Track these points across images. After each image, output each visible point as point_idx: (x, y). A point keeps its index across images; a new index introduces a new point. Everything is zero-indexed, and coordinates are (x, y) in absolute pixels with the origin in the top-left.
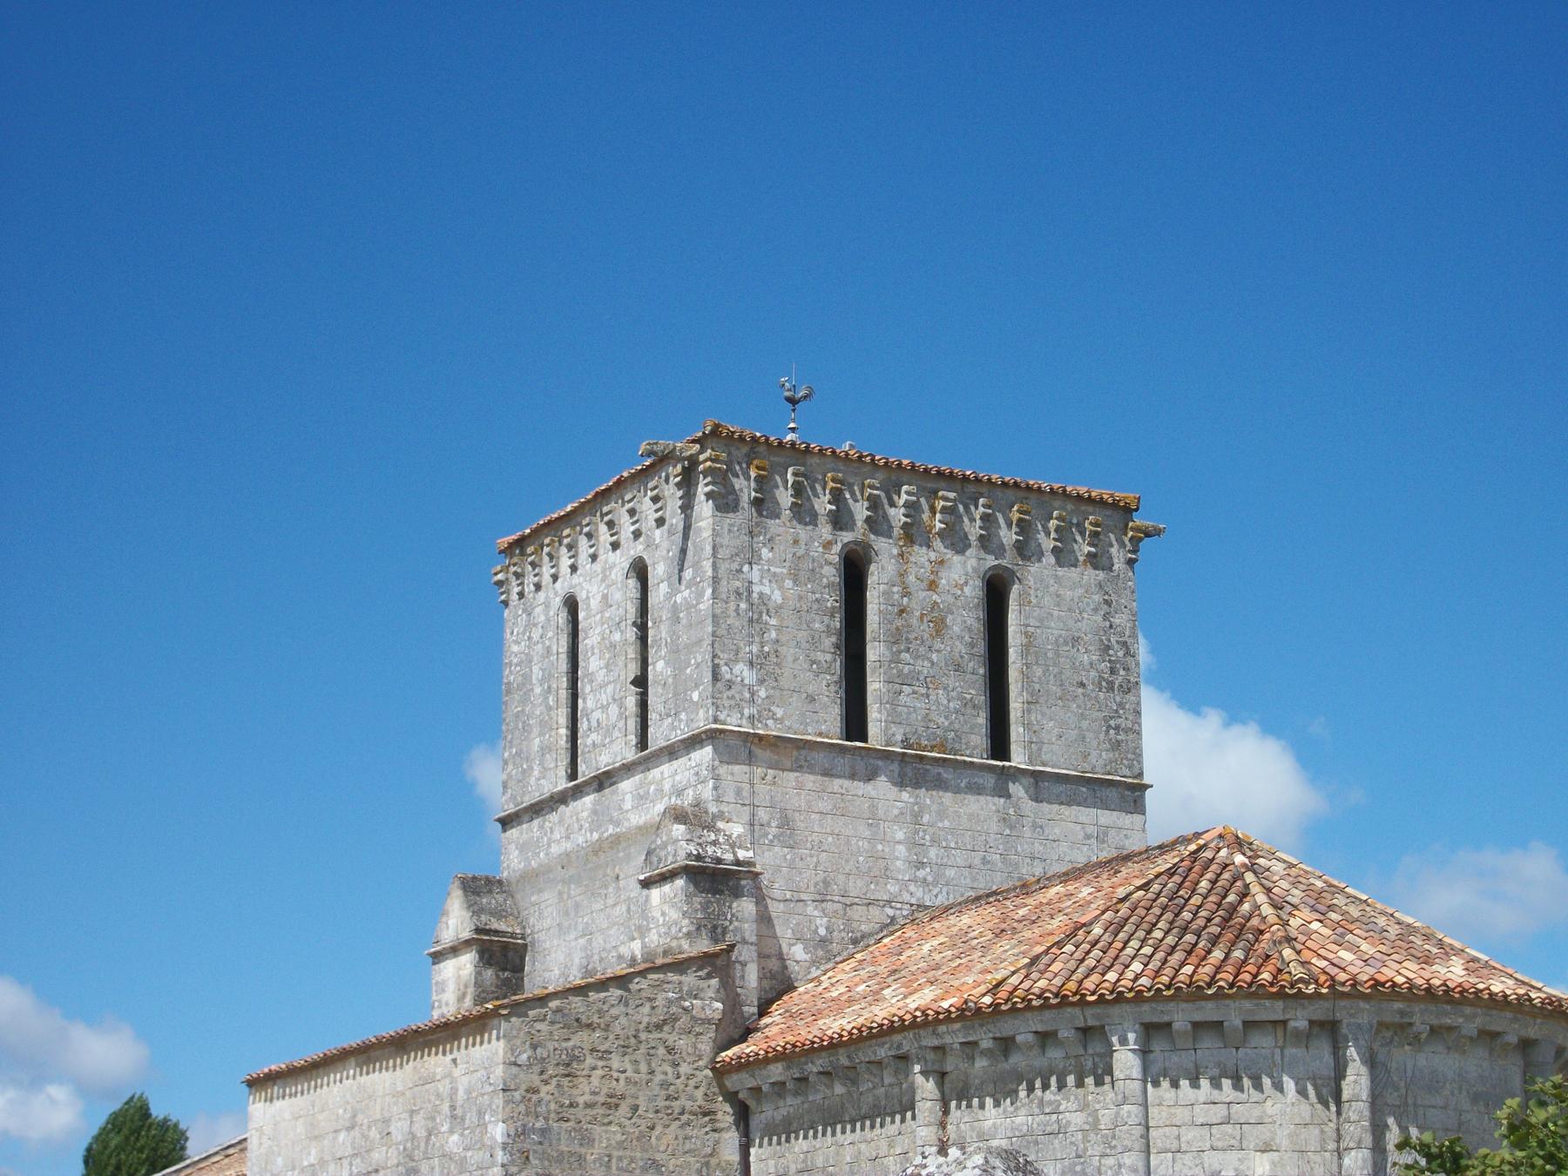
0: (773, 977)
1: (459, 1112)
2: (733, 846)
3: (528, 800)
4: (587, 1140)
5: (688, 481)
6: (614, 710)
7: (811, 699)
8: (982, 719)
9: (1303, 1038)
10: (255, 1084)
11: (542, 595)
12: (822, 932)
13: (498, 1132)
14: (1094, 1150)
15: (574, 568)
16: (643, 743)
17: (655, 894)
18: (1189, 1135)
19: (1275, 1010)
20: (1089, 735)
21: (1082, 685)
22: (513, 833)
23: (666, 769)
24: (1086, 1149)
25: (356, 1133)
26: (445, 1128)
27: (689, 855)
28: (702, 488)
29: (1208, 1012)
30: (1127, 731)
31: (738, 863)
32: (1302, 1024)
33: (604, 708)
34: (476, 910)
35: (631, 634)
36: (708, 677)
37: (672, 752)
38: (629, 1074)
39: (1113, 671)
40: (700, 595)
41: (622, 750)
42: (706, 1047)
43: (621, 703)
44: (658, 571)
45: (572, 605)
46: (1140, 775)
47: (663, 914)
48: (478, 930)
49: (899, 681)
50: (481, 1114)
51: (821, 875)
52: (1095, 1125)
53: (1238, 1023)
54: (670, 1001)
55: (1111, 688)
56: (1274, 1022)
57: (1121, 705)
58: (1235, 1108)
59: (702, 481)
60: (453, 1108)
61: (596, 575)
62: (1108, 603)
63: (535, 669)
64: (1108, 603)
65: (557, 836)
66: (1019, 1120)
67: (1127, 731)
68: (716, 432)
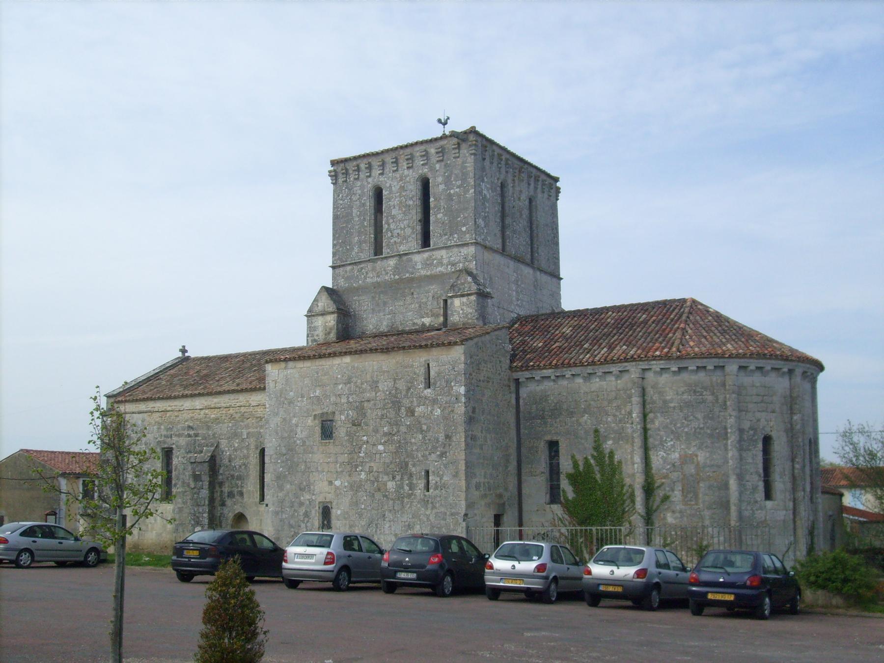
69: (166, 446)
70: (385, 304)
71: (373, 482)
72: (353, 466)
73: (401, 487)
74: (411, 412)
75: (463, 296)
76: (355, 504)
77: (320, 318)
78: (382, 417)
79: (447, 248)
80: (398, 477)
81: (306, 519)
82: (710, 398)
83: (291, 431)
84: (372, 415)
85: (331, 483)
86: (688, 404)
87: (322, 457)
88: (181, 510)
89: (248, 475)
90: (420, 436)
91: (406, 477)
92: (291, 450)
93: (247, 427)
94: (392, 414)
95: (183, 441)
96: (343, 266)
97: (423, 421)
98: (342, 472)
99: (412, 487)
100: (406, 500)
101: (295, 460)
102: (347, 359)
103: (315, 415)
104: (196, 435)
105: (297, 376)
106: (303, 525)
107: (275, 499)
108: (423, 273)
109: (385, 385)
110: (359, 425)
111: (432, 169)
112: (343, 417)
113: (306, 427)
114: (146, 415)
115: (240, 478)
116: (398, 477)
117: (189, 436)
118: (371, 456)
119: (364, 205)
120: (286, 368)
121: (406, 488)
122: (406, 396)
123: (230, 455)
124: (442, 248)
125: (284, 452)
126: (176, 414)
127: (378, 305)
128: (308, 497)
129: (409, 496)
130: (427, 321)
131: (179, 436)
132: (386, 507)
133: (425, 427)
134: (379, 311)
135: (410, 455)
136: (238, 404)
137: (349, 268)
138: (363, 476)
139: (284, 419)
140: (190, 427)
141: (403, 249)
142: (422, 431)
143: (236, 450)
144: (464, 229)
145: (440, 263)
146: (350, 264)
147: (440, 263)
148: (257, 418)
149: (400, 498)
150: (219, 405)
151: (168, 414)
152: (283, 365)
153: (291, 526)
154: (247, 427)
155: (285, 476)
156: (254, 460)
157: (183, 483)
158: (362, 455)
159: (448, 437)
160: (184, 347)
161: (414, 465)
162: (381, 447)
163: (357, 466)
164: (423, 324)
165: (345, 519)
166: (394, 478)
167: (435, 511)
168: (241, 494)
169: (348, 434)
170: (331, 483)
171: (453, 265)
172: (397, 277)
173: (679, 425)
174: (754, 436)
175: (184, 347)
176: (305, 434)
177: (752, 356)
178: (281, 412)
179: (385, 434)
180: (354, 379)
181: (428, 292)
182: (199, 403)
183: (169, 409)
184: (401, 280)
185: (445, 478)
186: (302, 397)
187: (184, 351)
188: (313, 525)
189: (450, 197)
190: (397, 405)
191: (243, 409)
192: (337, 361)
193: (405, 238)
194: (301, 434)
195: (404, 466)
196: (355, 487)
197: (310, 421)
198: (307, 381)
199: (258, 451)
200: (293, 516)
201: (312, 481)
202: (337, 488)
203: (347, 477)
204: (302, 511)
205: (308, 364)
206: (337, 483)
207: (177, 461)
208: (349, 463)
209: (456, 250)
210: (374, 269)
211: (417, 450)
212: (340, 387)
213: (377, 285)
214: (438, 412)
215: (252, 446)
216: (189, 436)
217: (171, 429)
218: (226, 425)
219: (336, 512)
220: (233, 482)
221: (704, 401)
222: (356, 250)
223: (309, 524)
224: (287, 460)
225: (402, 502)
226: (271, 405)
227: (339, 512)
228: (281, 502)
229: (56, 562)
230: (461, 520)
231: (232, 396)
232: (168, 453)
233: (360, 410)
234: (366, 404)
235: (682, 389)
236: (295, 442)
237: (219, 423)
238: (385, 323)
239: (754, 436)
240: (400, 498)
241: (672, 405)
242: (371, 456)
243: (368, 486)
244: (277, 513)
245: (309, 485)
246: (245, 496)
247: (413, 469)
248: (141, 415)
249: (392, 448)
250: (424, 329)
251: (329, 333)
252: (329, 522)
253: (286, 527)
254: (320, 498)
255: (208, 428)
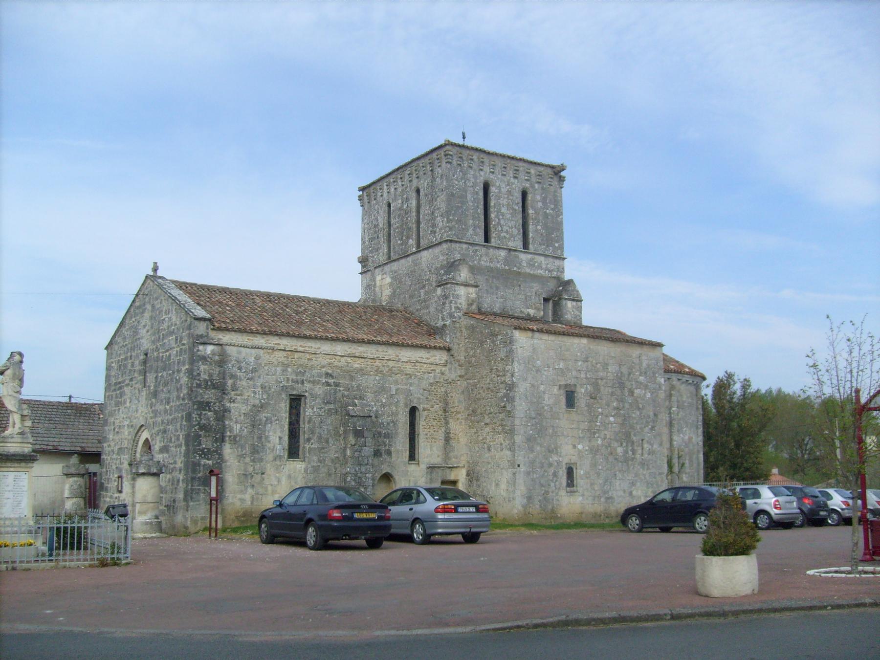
69: (295, 393)
70: (497, 288)
71: (607, 447)
72: (592, 433)
73: (626, 452)
74: (631, 393)
75: (573, 300)
76: (594, 465)
77: (462, 287)
78: (612, 394)
79: (546, 256)
80: (624, 444)
81: (555, 479)
83: (540, 397)
84: (605, 391)
85: (574, 446)
87: (568, 424)
88: (316, 469)
89: (397, 434)
90: (638, 413)
91: (630, 444)
92: (540, 415)
93: (396, 382)
94: (618, 392)
95: (319, 390)
96: (460, 242)
97: (639, 400)
98: (583, 437)
99: (634, 452)
100: (630, 463)
101: (544, 424)
102: (584, 341)
103: (560, 385)
104: (337, 385)
105: (543, 347)
106: (552, 484)
107: (526, 459)
108: (528, 270)
109: (612, 368)
110: (595, 399)
111: (532, 186)
112: (583, 390)
113: (553, 397)
114: (261, 352)
115: (387, 436)
116: (624, 444)
117: (328, 384)
118: (605, 425)
119: (477, 193)
120: (532, 337)
121: (630, 453)
122: (628, 379)
123: (377, 411)
124: (542, 255)
125: (534, 416)
126: (308, 356)
127: (491, 287)
128: (556, 459)
129: (633, 459)
130: (532, 312)
131: (313, 382)
132: (617, 468)
133: (641, 406)
134: (493, 293)
135: (632, 427)
136: (386, 358)
137: (465, 246)
138: (600, 442)
139: (533, 385)
140: (327, 375)
141: (511, 244)
142: (639, 409)
143: (383, 406)
144: (557, 245)
145: (540, 267)
146: (466, 243)
147: (540, 267)
148: (406, 374)
149: (626, 461)
150: (365, 355)
151: (296, 355)
152: (530, 334)
153: (542, 485)
154: (396, 382)
155: (535, 439)
156: (403, 418)
157: (320, 437)
158: (598, 424)
159: (655, 415)
161: (635, 435)
162: (612, 419)
163: (595, 433)
164: (529, 314)
165: (587, 478)
166: (621, 444)
168: (389, 453)
169: (588, 405)
170: (574, 446)
171: (549, 271)
172: (507, 268)
176: (551, 401)
178: (530, 379)
179: (615, 408)
180: (590, 359)
181: (532, 288)
182: (341, 349)
183: (300, 349)
184: (510, 272)
185: (655, 446)
186: (549, 367)
187: (155, 269)
188: (561, 484)
189: (546, 215)
190: (622, 386)
191: (391, 364)
192: (576, 340)
193: (512, 236)
194: (548, 400)
195: (628, 435)
196: (594, 451)
197: (555, 390)
198: (552, 353)
199: (408, 410)
200: (543, 476)
201: (559, 443)
202: (580, 451)
203: (588, 443)
204: (552, 470)
205: (552, 338)
206: (580, 447)
207: (308, 411)
208: (589, 430)
209: (551, 260)
210: (487, 255)
211: (637, 423)
212: (580, 363)
213: (490, 270)
214: (649, 395)
215: (402, 404)
216: (328, 384)
217: (303, 374)
218: (372, 378)
219: (579, 472)
220: (380, 440)
222: (471, 232)
223: (557, 483)
224: (537, 423)
225: (628, 465)
226: (519, 370)
227: (582, 472)
228: (532, 463)
229: (660, 528)
230: (665, 478)
231: (381, 348)
232: (296, 402)
233: (596, 385)
234: (600, 381)
236: (543, 407)
237: (364, 374)
238: (498, 305)
240: (626, 461)
242: (605, 425)
243: (603, 450)
244: (528, 473)
245: (556, 448)
246: (393, 455)
247: (634, 438)
248: (253, 351)
249: (620, 420)
250: (529, 318)
251: (471, 304)
252: (572, 481)
253: (537, 487)
254: (566, 460)
255: (352, 378)
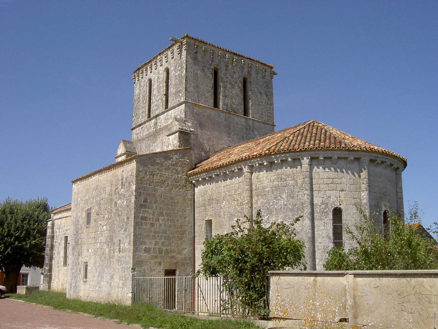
0: (197, 159)
1: (124, 183)
2: (189, 127)
3: (138, 124)
4: (155, 190)
5: (180, 48)
6: (160, 101)
7: (206, 97)
8: (242, 107)
9: (352, 162)
10: (74, 182)
11: (143, 80)
12: (208, 149)
13: (134, 187)
14: (296, 190)
15: (151, 72)
16: (167, 106)
17: (171, 137)
18: (322, 187)
19: (345, 154)
20: (264, 114)
21: (262, 103)
22: (134, 131)
23: (172, 111)
24: (294, 190)
25: (97, 191)
26: (120, 187)
27: (179, 128)
28: (184, 47)
29: (328, 154)
30: (271, 114)
31: (191, 131)
32: (352, 158)
33: (158, 101)
34: (125, 146)
35: (165, 84)
36: (184, 90)
37: (174, 107)
38: (167, 175)
39: (268, 101)
40: (182, 72)
41: (162, 109)
42: (185, 169)
43: (162, 99)
44: (172, 69)
45: (150, 81)
46: (273, 123)
47: (173, 142)
48: (126, 151)
49: (225, 96)
50: (129, 183)
51: (208, 137)
52: (297, 185)
53: (336, 157)
54: (177, 158)
55: (268, 104)
56: (344, 158)
57: (270, 108)
58: (334, 180)
59: (184, 46)
60: (122, 183)
61: (156, 74)
62: (267, 86)
63: (141, 95)
64: (267, 86)
65: (145, 131)
66: (274, 183)
67: (271, 114)
68: (187, 36)
82: (291, 182)
86: (277, 188)
102: (97, 176)
111: (170, 64)
160: (277, 74)
167: (121, 266)
173: (271, 204)
174: (325, 208)
175: (277, 74)
177: (323, 149)
221: (287, 185)
235: (273, 178)
239: (325, 208)
241: (267, 189)
